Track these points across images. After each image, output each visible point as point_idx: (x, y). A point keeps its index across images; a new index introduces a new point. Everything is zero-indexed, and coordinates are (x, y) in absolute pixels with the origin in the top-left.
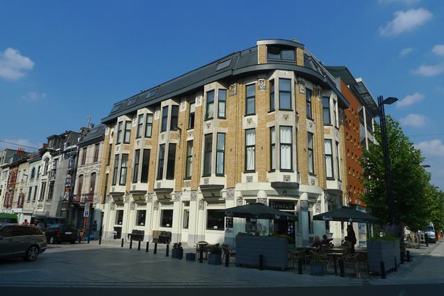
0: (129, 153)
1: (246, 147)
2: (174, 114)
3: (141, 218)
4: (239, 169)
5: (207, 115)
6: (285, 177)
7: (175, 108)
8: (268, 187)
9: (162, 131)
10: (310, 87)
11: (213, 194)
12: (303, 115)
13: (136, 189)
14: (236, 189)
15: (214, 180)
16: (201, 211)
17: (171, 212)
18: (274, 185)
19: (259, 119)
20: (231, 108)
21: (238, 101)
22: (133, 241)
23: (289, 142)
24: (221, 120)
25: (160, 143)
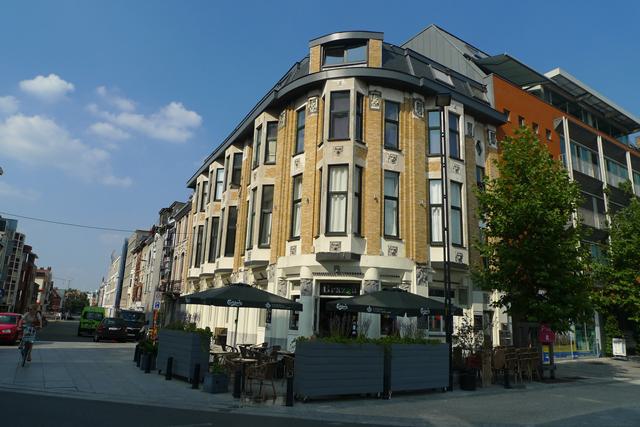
1: (330, 195)
2: (236, 167)
4: (283, 237)
6: (332, 244)
7: (238, 156)
8: (312, 260)
9: (296, 154)
10: (396, 97)
13: (220, 267)
14: (278, 266)
18: (322, 258)
23: (344, 189)
25: (293, 173)
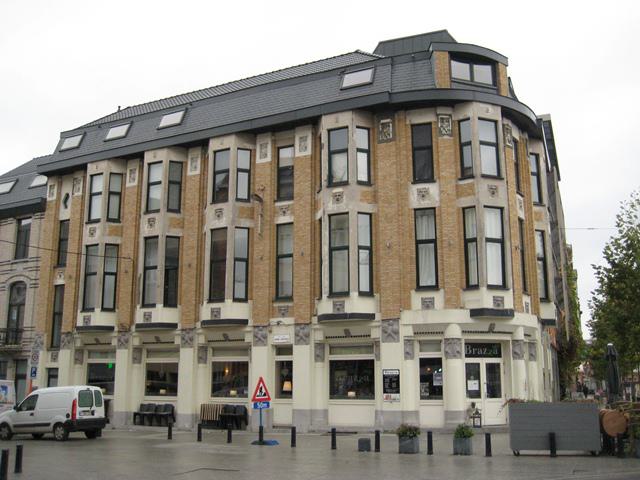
0: (119, 242)
1: (418, 242)
3: (162, 380)
5: (330, 176)
8: (464, 316)
11: (157, 338)
12: (513, 188)
14: (401, 322)
15: (231, 310)
16: (319, 364)
17: (289, 364)
19: (441, 192)
20: (385, 166)
21: (398, 154)
22: (203, 431)
24: (112, 224)
